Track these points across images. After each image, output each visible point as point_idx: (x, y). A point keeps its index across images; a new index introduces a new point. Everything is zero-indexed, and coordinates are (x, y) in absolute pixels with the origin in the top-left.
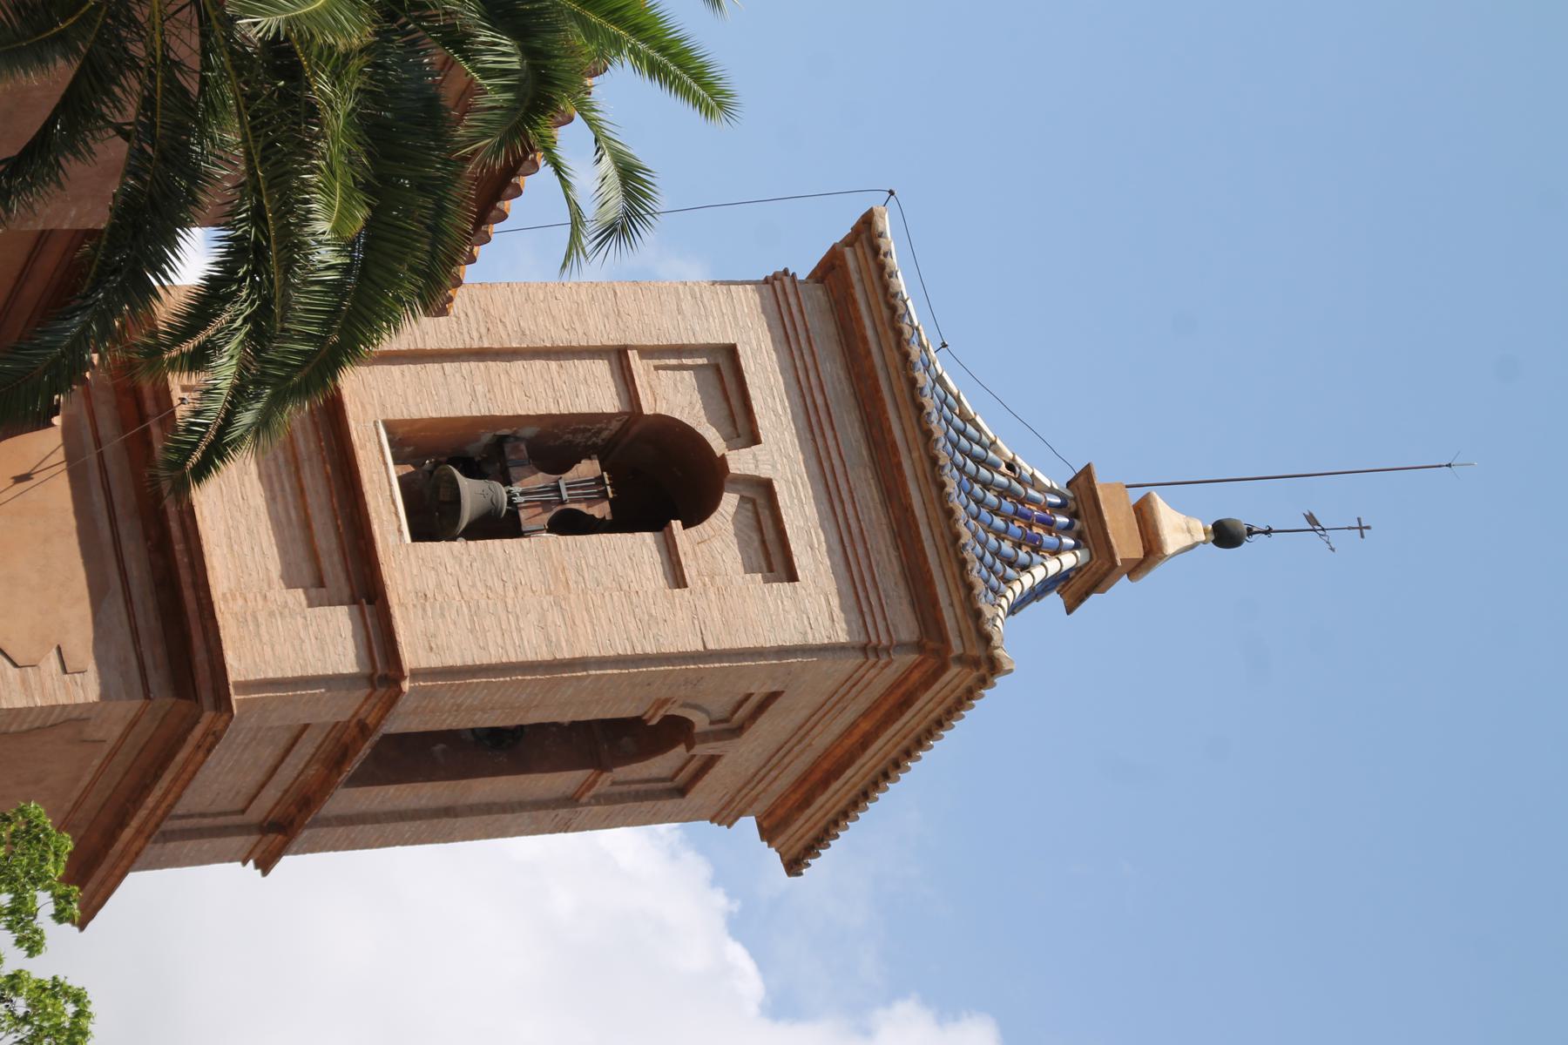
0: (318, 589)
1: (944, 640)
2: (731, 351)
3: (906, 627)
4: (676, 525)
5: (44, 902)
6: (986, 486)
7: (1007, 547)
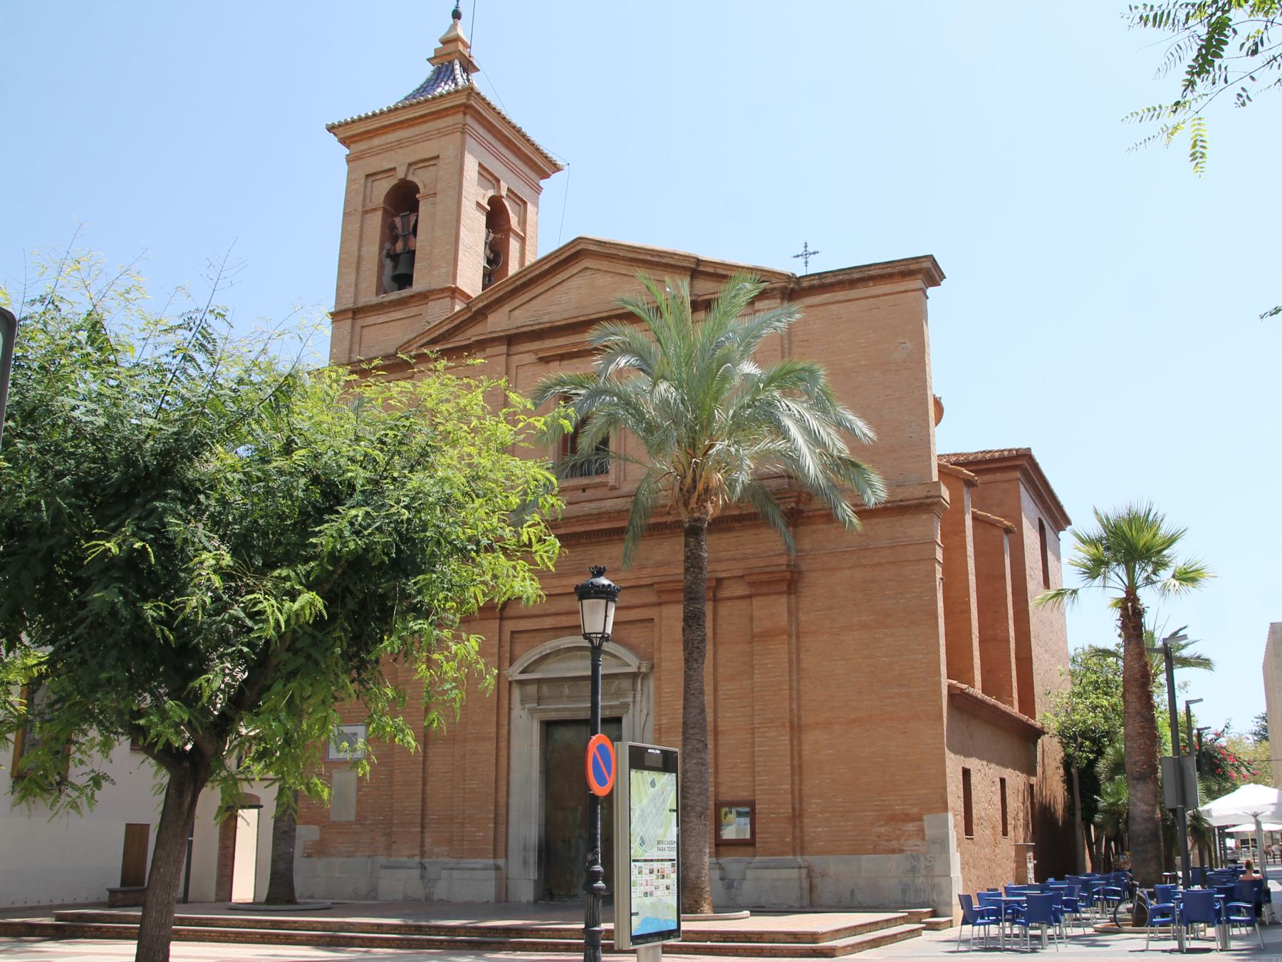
2: (367, 176)
4: (418, 196)
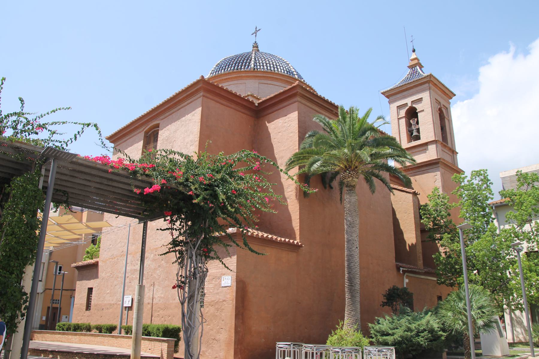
0: (426, 149)
1: (428, 81)
2: (397, 107)
3: (427, 85)
4: (417, 111)
5: (463, 176)
6: (410, 78)
7: (417, 75)
